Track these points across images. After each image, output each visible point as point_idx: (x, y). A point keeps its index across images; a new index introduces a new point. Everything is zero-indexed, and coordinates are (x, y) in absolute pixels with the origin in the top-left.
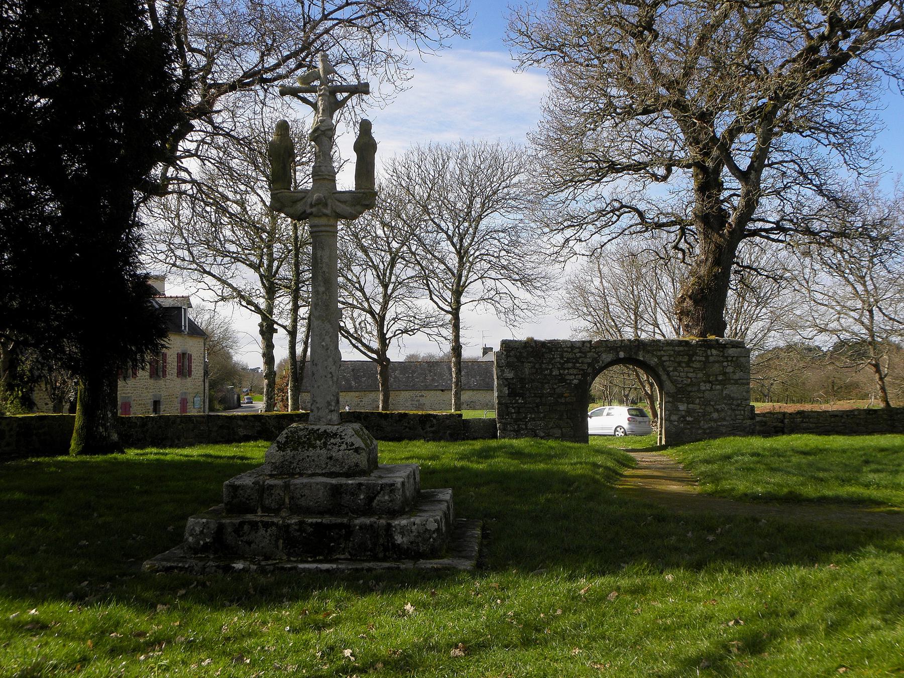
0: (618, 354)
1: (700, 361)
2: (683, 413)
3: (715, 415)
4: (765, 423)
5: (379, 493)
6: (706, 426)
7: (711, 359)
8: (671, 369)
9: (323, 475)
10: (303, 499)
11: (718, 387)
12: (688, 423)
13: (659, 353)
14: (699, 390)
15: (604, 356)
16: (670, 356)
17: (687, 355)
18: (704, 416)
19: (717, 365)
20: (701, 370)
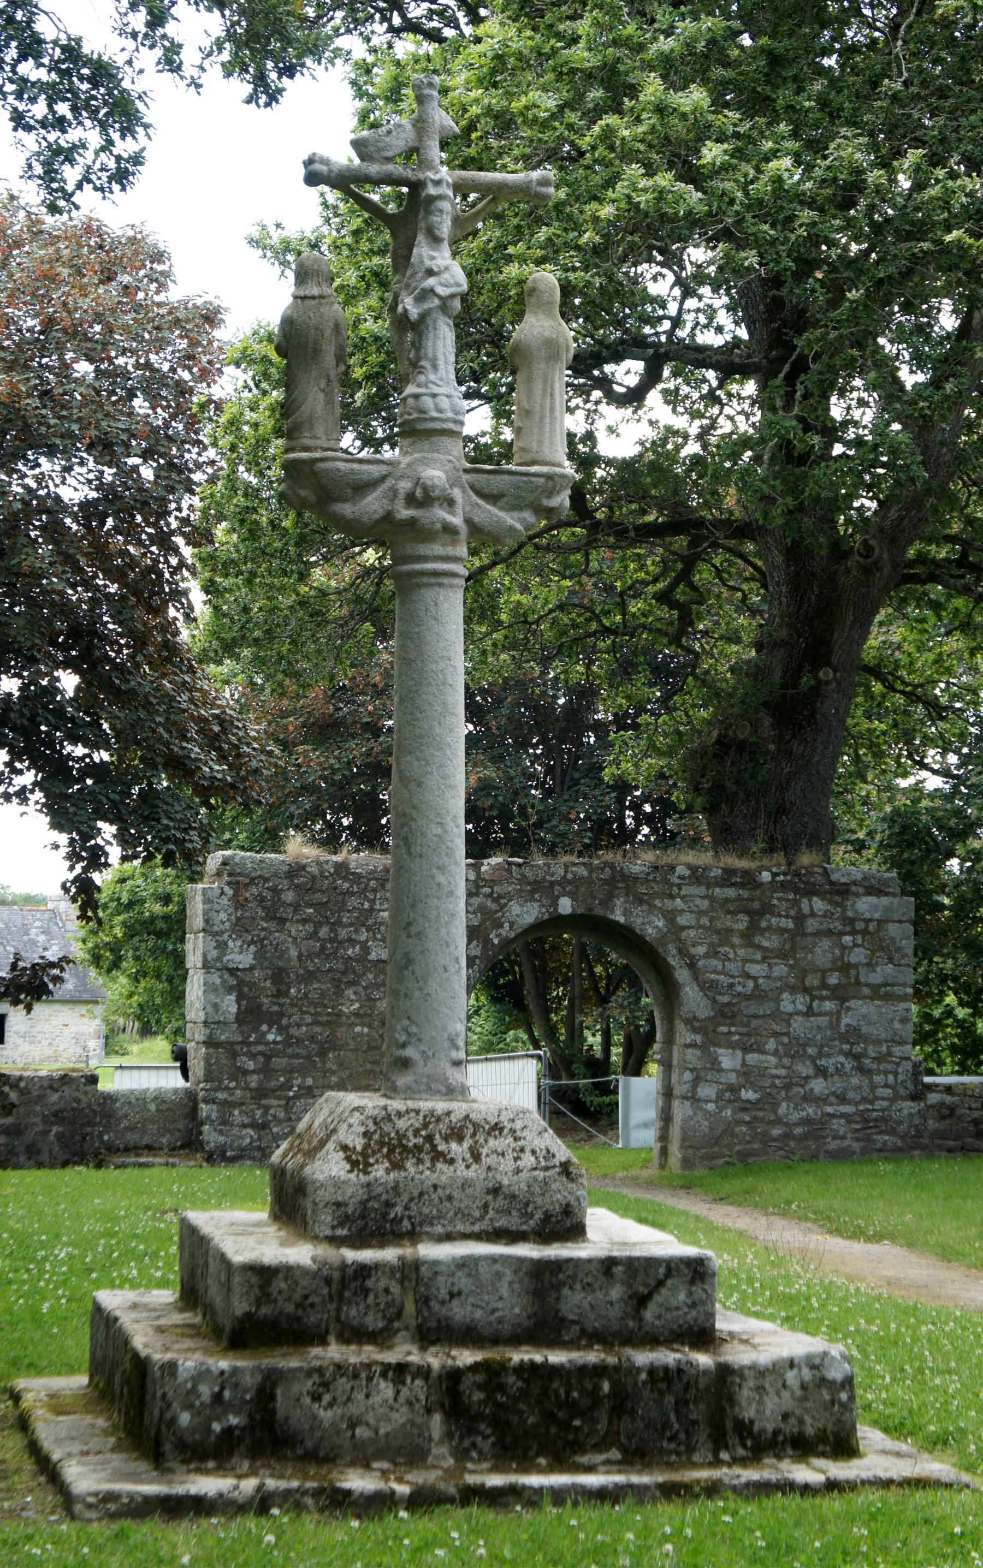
0: (555, 903)
1: (782, 931)
2: (733, 1078)
3: (818, 1086)
4: (952, 1109)
5: (661, 1283)
6: (795, 1116)
7: (811, 925)
8: (701, 950)
9: (477, 1237)
10: (455, 1302)
11: (828, 1005)
12: (747, 1106)
13: (669, 904)
14: (776, 1015)
15: (515, 908)
16: (701, 913)
17: (749, 912)
18: (788, 1087)
19: (826, 943)
20: (783, 955)
